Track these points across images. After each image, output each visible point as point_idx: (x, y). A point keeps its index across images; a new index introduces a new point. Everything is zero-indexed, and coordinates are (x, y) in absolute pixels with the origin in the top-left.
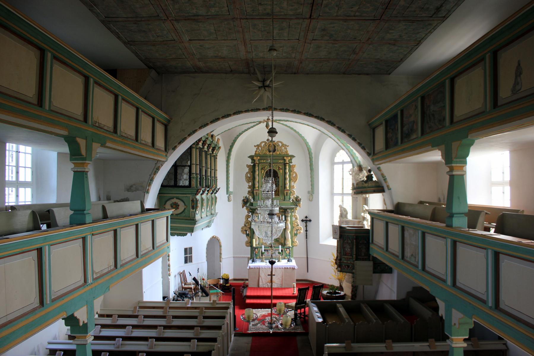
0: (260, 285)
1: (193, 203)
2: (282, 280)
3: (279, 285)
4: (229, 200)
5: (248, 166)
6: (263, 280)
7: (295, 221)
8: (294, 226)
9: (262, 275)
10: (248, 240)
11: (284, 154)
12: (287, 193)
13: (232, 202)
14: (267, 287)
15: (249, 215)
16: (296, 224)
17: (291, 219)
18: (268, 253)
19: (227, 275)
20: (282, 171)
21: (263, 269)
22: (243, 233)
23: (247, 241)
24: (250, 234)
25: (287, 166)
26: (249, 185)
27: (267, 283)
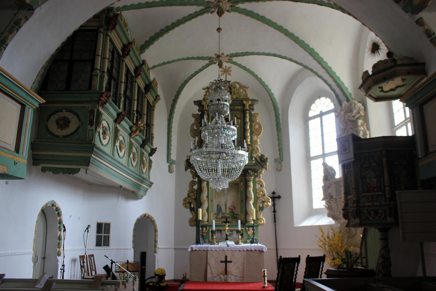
0: (208, 278)
1: (92, 115)
2: (244, 269)
3: (238, 278)
4: (170, 171)
5: (194, 116)
6: (213, 269)
8: (258, 196)
9: (212, 261)
10: (193, 217)
11: (243, 98)
13: (174, 174)
14: (219, 281)
15: (193, 181)
16: (262, 193)
17: (254, 185)
18: (221, 235)
19: (161, 270)
20: (241, 122)
21: (212, 251)
22: (186, 207)
23: (191, 218)
24: (195, 207)
25: (247, 113)
27: (219, 275)
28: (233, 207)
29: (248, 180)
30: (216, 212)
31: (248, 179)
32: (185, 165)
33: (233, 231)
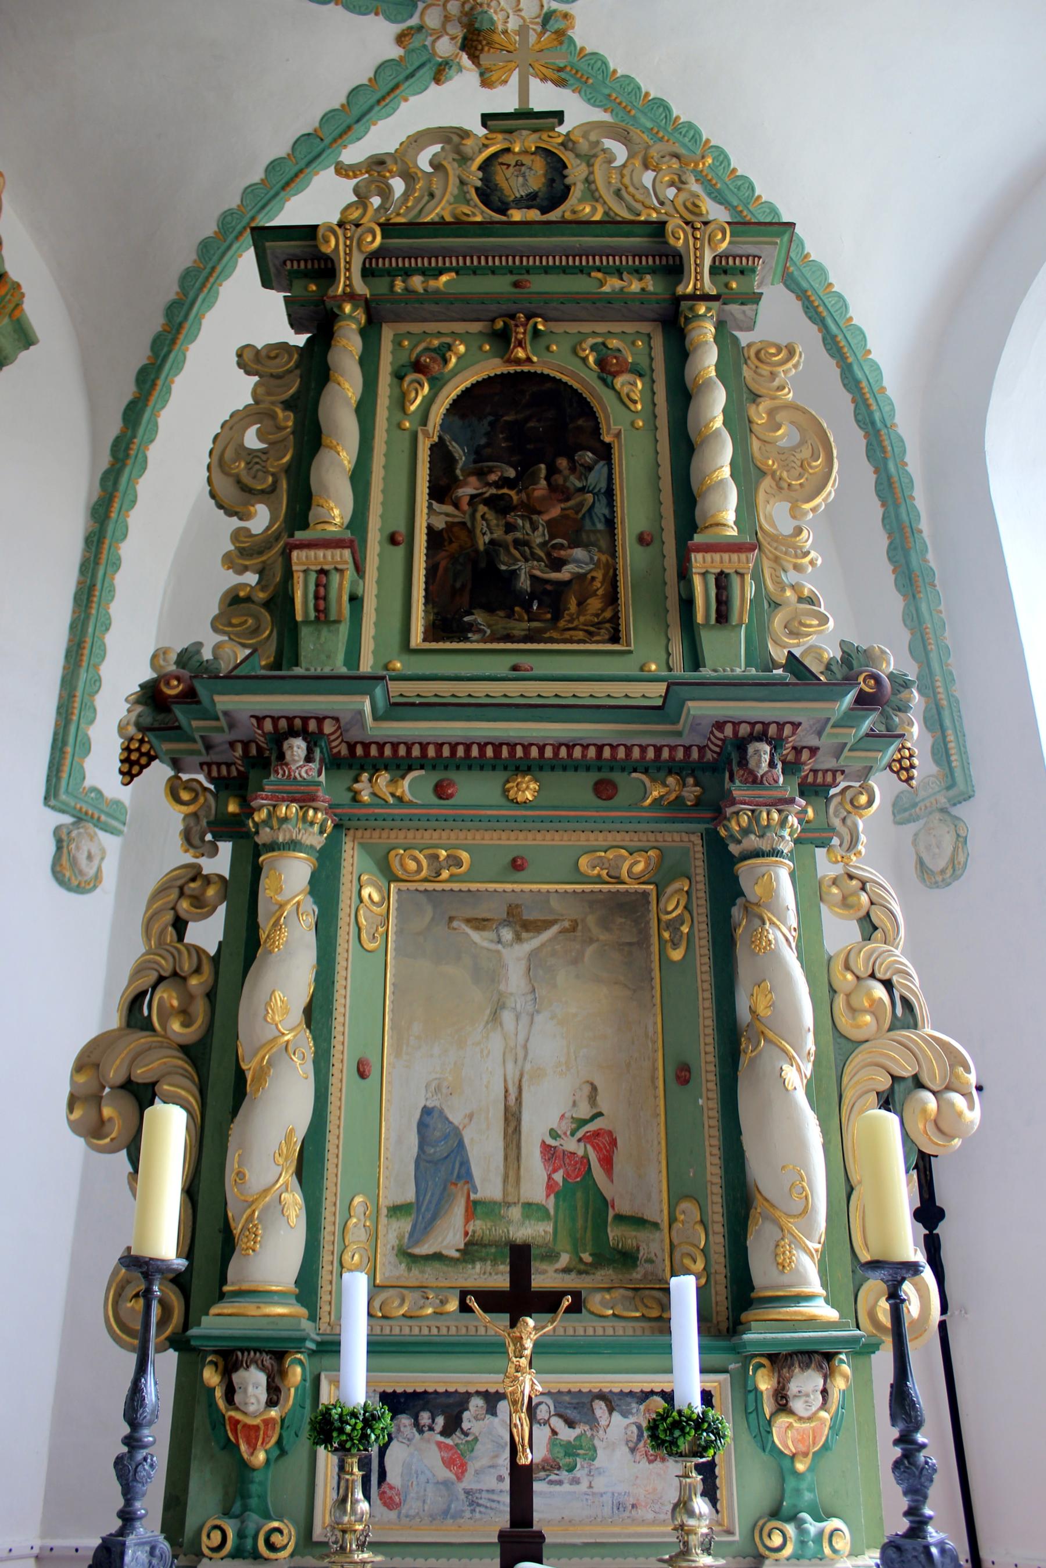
7: (861, 966)
8: (844, 1022)
12: (722, 581)
15: (196, 874)
16: (880, 992)
18: (457, 1463)
26: (237, 535)
28: (590, 1138)
29: (752, 841)
30: (409, 1195)
31: (746, 832)
32: (121, 729)
33: (600, 1409)
